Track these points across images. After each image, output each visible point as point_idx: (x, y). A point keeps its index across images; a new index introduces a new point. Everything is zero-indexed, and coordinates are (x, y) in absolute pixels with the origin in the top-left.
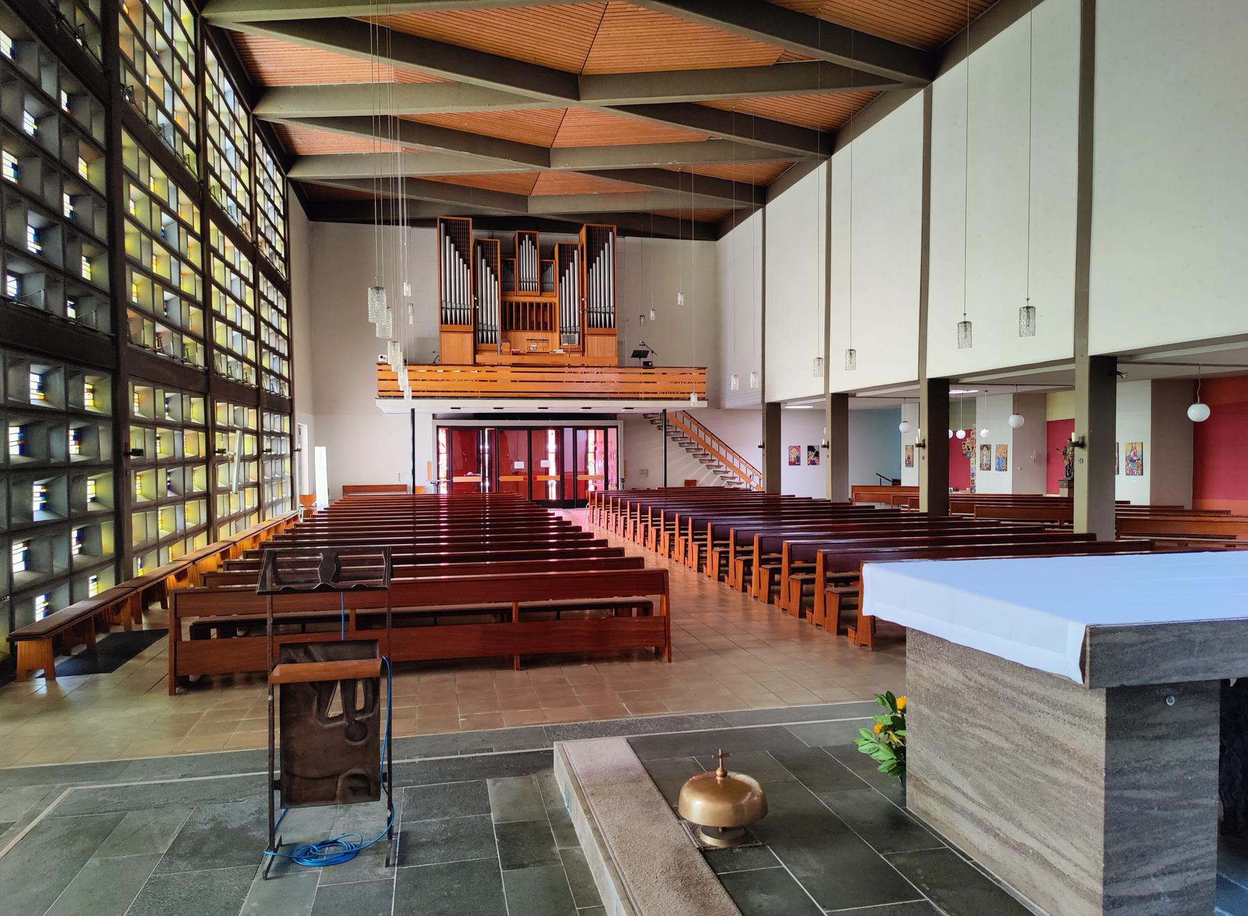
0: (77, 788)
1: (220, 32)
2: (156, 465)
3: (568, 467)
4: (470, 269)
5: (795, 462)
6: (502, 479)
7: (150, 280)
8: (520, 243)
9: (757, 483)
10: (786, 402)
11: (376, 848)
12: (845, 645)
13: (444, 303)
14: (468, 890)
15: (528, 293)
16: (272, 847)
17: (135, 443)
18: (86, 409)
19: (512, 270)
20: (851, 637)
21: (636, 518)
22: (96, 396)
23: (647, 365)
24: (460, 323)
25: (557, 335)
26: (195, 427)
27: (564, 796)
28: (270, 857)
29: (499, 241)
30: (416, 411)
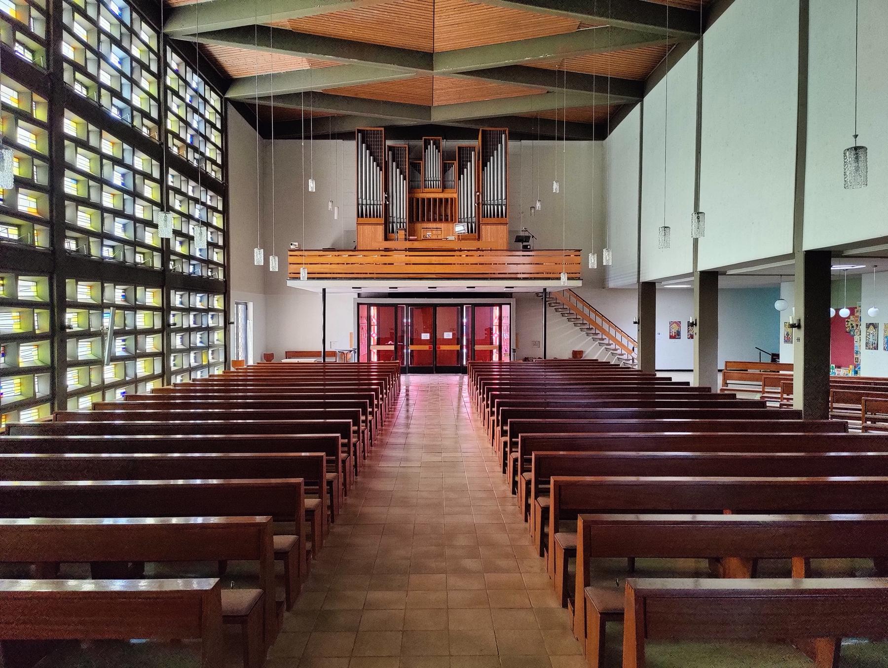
4: (382, 171)
5: (676, 336)
8: (426, 148)
13: (360, 200)
15: (432, 190)
24: (374, 217)
30: (327, 291)
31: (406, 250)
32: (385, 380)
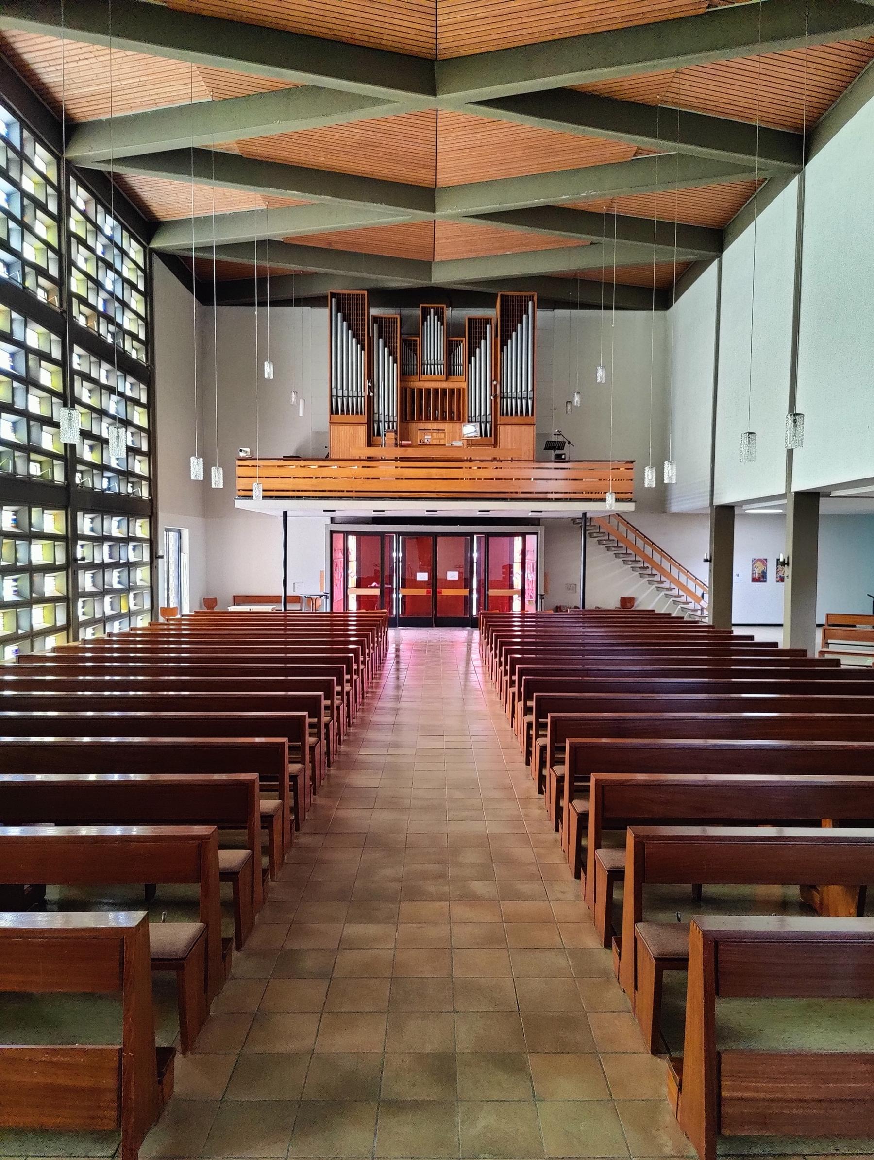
5: (760, 578)
8: (424, 319)
19: (415, 351)
24: (353, 413)
31: (396, 459)
32: (367, 636)
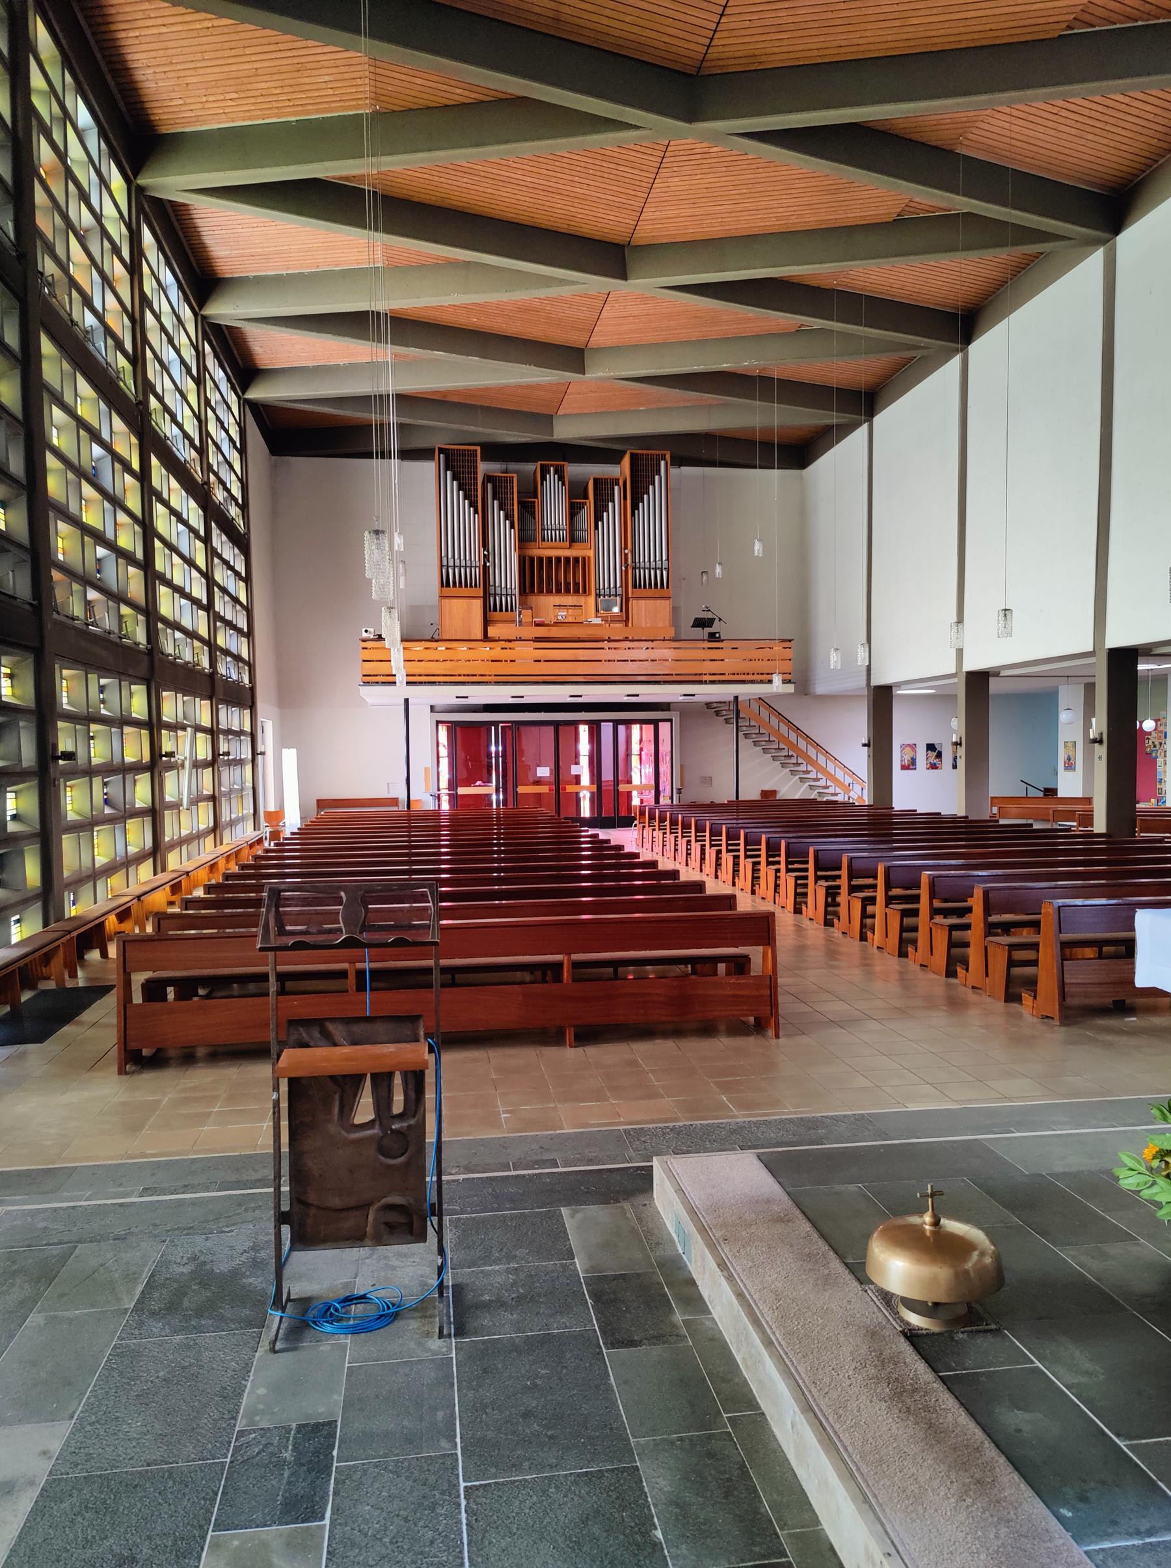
0: (9, 1208)
1: (159, 204)
2: (90, 772)
3: (607, 775)
5: (910, 765)
6: (521, 789)
7: (79, 532)
8: (543, 478)
9: (861, 794)
10: (900, 685)
11: (422, 1308)
12: (1020, 1016)
13: (444, 560)
14: (561, 1380)
15: (554, 544)
16: (278, 1302)
17: (65, 744)
18: (4, 699)
19: (533, 514)
20: (1027, 1006)
21: (705, 841)
22: (15, 683)
23: (713, 637)
24: (466, 586)
25: (591, 600)
26: (137, 723)
27: (675, 1236)
28: (277, 1320)
29: (515, 476)
